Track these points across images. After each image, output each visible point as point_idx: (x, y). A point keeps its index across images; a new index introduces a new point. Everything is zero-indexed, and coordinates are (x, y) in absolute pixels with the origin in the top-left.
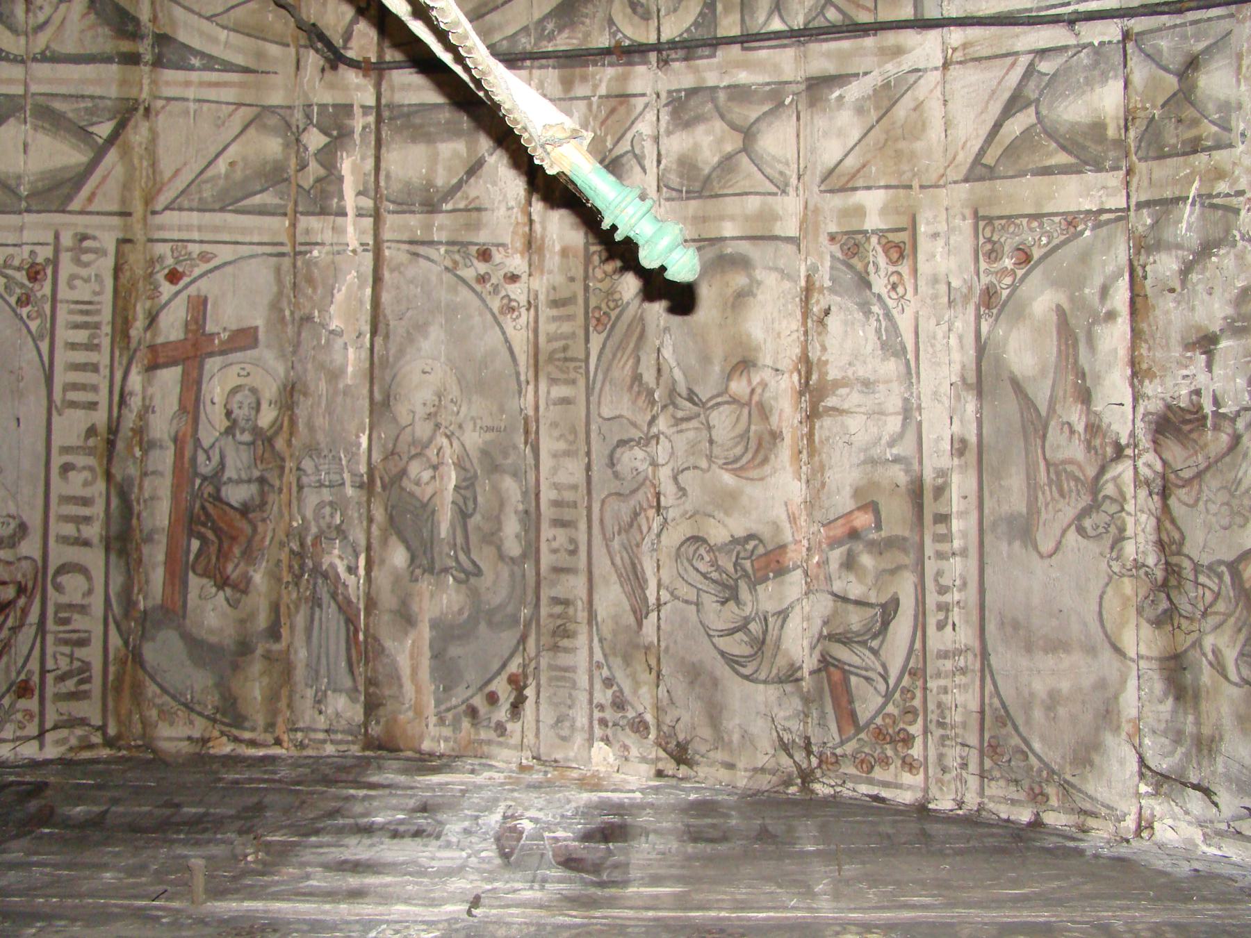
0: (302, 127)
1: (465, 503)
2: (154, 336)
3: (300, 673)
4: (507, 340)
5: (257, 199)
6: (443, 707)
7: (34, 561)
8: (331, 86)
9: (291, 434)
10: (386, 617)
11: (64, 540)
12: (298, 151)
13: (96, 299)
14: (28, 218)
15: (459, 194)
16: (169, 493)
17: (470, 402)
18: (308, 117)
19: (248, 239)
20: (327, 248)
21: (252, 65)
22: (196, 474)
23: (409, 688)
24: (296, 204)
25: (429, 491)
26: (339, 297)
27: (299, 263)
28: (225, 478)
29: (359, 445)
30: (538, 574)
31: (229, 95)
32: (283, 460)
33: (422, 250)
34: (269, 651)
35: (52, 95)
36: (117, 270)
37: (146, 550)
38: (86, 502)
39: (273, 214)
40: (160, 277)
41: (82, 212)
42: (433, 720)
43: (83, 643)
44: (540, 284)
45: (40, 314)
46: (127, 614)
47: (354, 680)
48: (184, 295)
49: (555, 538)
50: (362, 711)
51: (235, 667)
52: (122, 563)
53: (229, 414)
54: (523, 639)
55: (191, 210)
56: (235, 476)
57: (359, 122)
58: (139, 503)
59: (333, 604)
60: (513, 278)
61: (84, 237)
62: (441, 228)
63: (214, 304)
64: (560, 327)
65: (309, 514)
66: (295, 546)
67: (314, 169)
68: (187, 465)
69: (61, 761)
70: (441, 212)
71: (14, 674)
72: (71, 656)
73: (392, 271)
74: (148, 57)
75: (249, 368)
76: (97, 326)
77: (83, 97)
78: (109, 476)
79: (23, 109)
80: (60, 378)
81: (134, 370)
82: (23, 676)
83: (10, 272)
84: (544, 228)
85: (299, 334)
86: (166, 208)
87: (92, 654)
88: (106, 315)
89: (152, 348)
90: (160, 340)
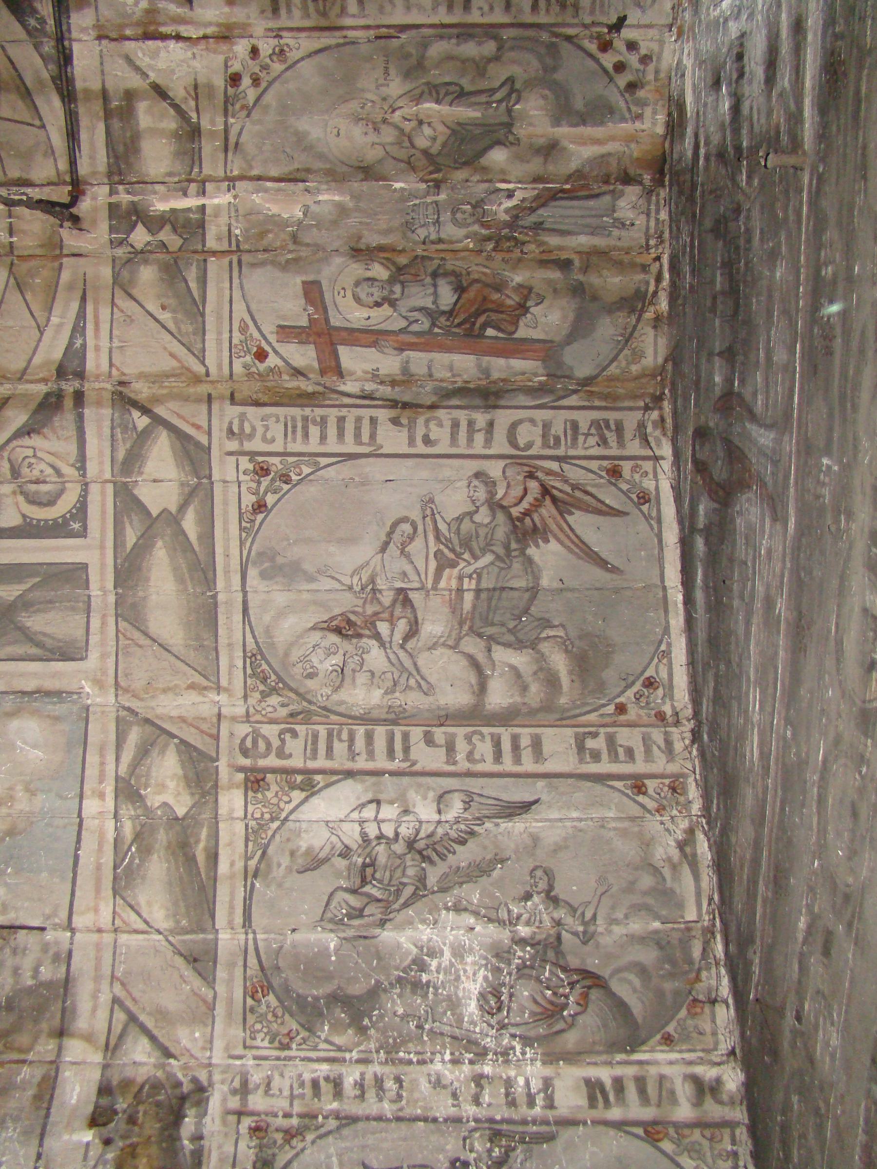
0: (130, 249)
1: (453, 93)
2: (312, 370)
3: (599, 242)
4: (309, 56)
5: (193, 285)
6: (627, 116)
7: (506, 465)
8: (94, 222)
9: (394, 250)
10: (551, 168)
11: (488, 442)
12: (151, 252)
13: (282, 419)
14: (216, 476)
15: (183, 106)
16: (447, 355)
17: (363, 90)
18: (121, 243)
19: (228, 292)
20: (233, 222)
21: (78, 294)
22: (430, 332)
23: (610, 147)
24: (195, 252)
25: (441, 128)
26: (274, 209)
27: (247, 247)
28: (433, 307)
29: (402, 189)
30: (512, 25)
31: (105, 313)
32: (416, 257)
33: (232, 140)
34: (581, 269)
35: (112, 461)
36: (257, 404)
37: (495, 375)
38: (455, 425)
39: (205, 270)
40: (262, 367)
41: (209, 434)
42: (638, 125)
43: (575, 426)
44: (259, 26)
45: (297, 465)
46: (551, 391)
47: (604, 193)
48: (275, 344)
49: (481, 9)
50: (630, 187)
51: (595, 298)
52: (507, 395)
53: (378, 304)
54: (569, 39)
55: (204, 341)
56: (431, 299)
57: (124, 197)
58: (456, 382)
59: (540, 212)
60: (255, 52)
61: (231, 432)
62: (213, 122)
63: (284, 318)
64: (295, 5)
65: (462, 232)
66: (490, 246)
67: (166, 235)
68: (423, 340)
69: (674, 442)
70: (199, 123)
71: (602, 481)
72: (587, 435)
73: (251, 167)
74: (77, 384)
75: (338, 288)
76: (305, 419)
77: (112, 436)
78: (433, 407)
79: (125, 484)
80: (350, 447)
81: (342, 388)
82: (604, 474)
83: (262, 489)
84: (210, 24)
85: (308, 245)
86: (203, 363)
87: (584, 419)
88: (296, 412)
89: (323, 372)
90: (316, 365)
